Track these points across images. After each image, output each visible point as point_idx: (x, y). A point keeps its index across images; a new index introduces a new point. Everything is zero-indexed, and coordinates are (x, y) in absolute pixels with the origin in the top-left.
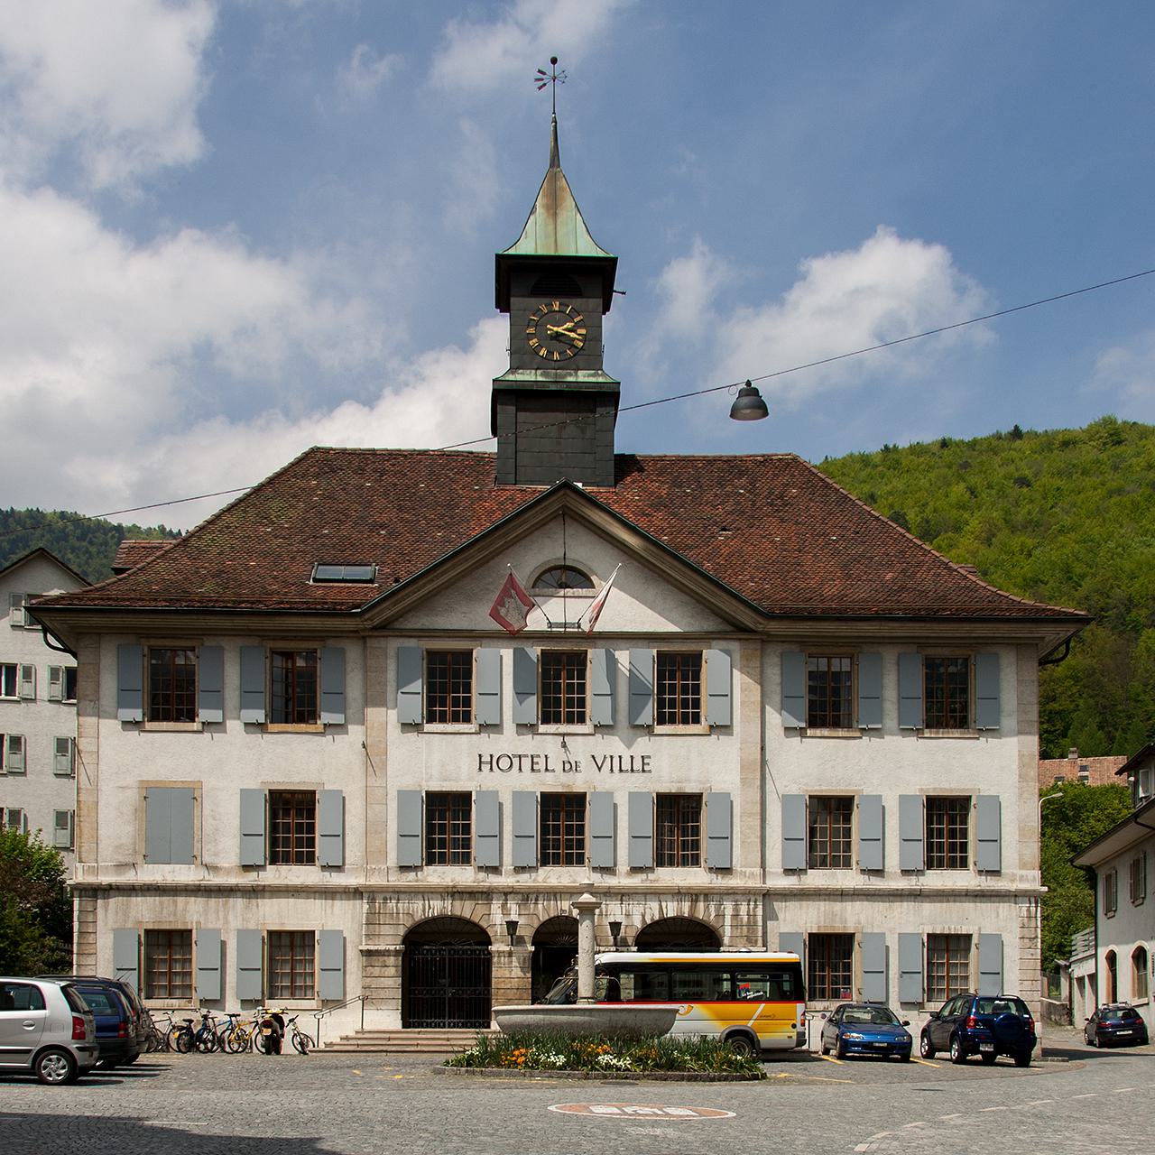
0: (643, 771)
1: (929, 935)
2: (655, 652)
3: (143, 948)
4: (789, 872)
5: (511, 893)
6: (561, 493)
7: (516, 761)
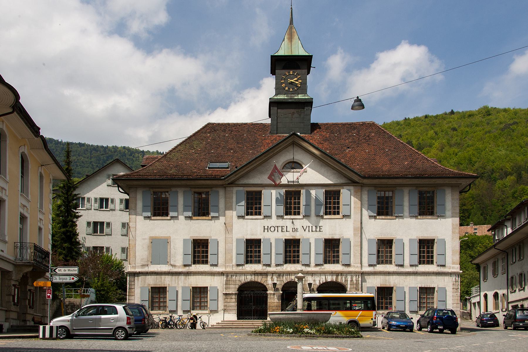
0: (320, 231)
3: (150, 293)
5: (274, 273)
6: (293, 136)
7: (276, 228)
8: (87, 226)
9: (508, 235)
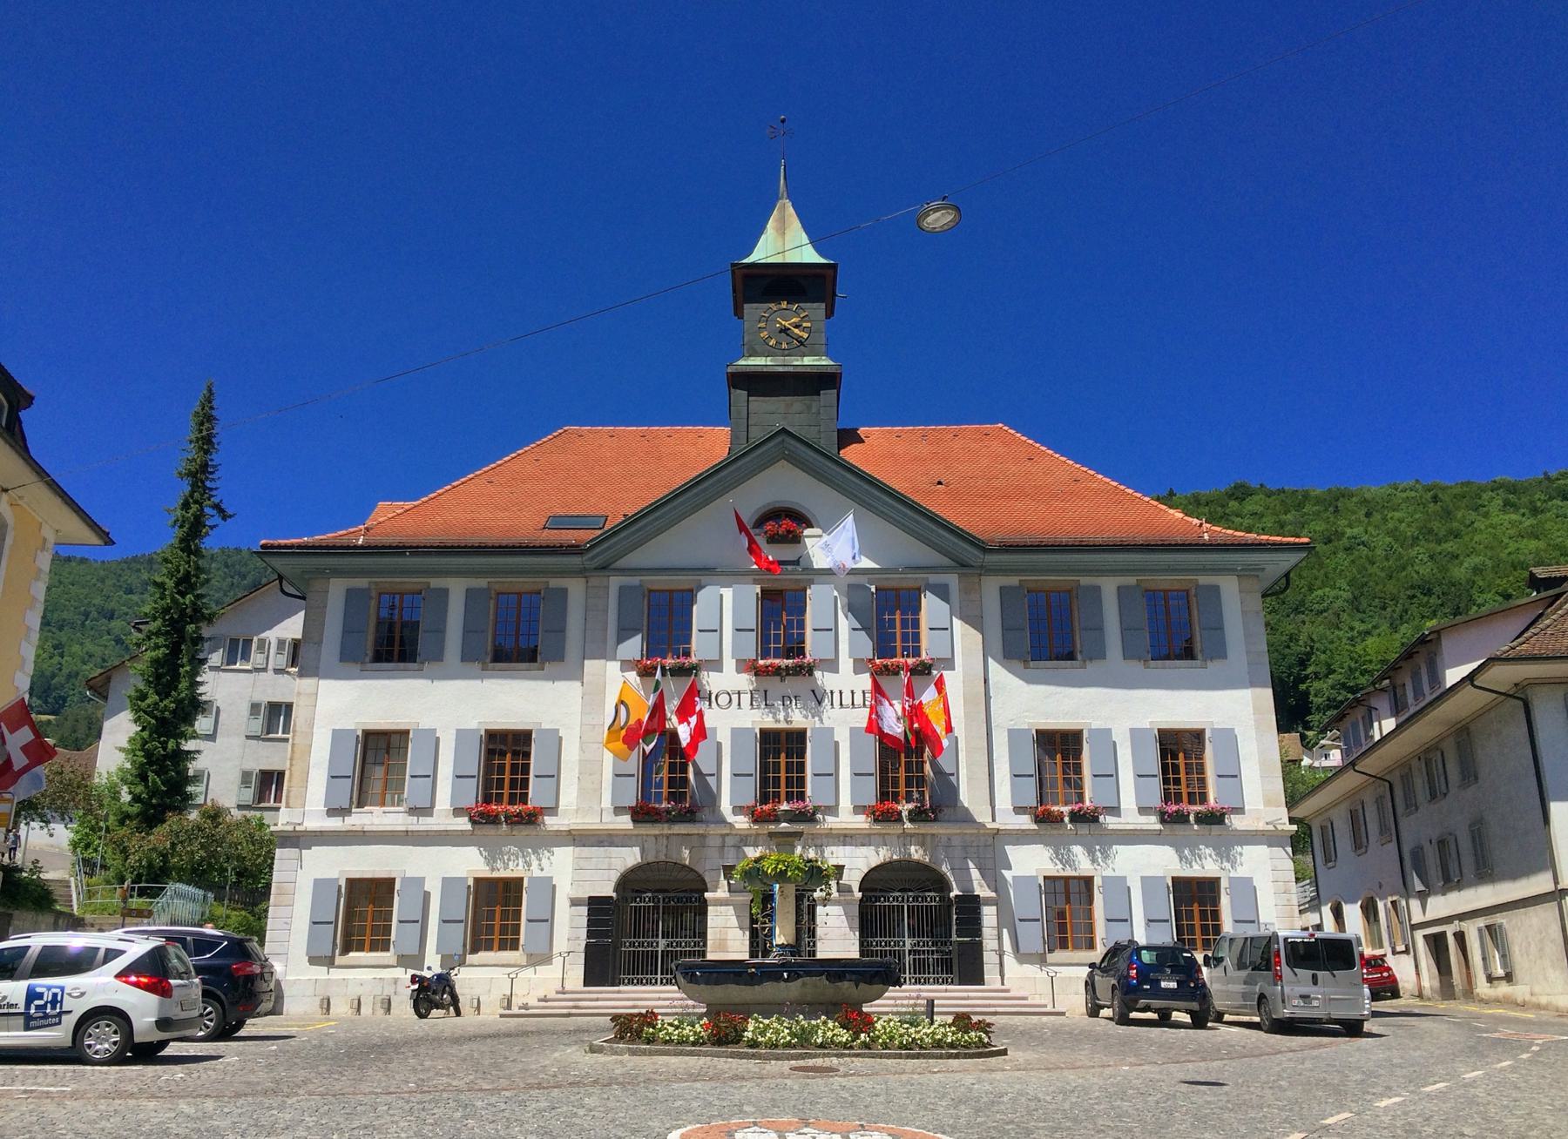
1: (1174, 879)
2: (759, 590)
3: (342, 899)
4: (332, 812)
6: (779, 439)
7: (735, 697)
8: (251, 715)
9: (1384, 734)
